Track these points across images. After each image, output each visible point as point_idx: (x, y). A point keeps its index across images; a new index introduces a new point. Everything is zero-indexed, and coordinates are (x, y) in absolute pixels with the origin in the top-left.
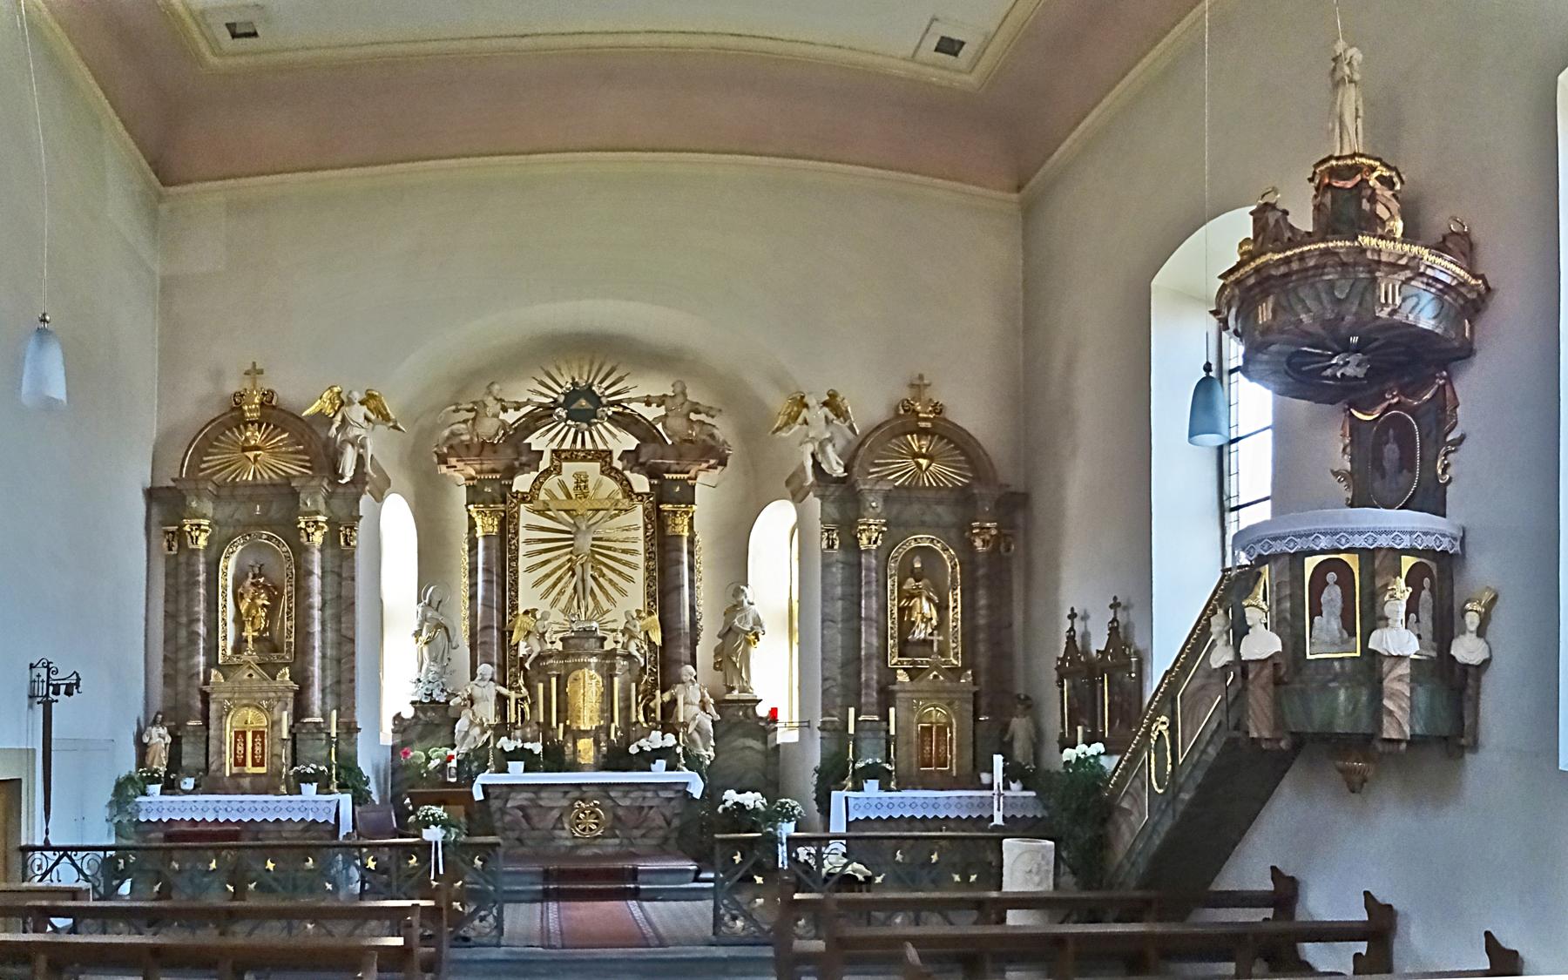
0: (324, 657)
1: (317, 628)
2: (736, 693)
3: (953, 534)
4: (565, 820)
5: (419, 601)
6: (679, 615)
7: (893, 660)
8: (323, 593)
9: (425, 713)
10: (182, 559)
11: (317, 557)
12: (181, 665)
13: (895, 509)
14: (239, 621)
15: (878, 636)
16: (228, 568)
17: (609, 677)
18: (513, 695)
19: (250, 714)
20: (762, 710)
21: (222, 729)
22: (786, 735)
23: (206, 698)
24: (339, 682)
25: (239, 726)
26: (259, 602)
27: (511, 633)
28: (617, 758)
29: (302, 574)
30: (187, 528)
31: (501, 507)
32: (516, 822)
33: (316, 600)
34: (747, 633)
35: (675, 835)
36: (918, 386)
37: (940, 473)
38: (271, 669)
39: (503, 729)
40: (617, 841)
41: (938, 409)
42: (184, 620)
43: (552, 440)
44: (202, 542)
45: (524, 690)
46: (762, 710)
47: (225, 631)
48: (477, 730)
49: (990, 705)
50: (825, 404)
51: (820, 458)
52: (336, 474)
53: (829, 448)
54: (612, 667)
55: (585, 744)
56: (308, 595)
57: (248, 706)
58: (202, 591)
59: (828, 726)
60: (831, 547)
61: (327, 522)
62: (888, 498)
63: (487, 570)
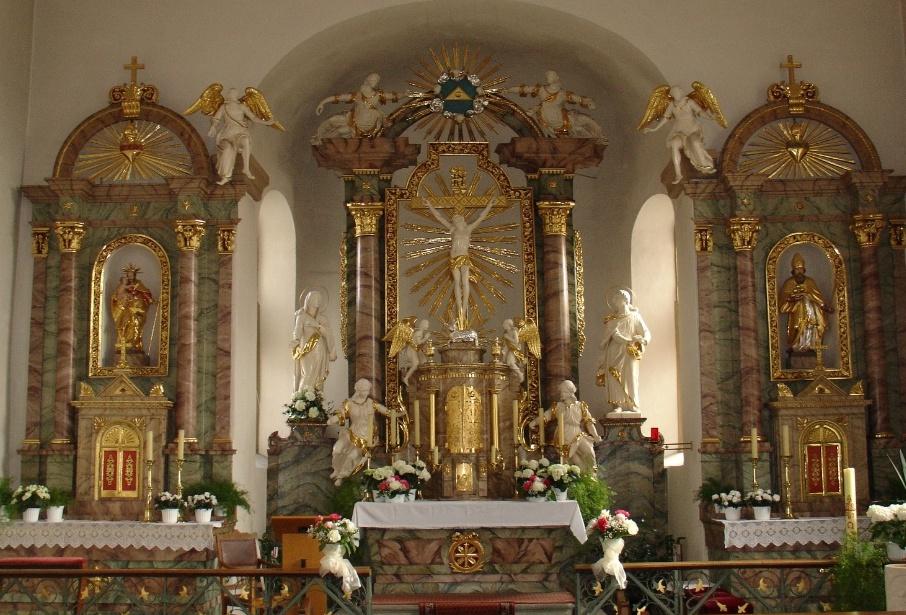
0: (199, 371)
1: (193, 339)
2: (619, 411)
3: (837, 228)
4: (445, 554)
5: (297, 309)
6: (558, 321)
7: (776, 373)
8: (199, 301)
9: (302, 434)
10: (53, 262)
11: (193, 263)
12: (49, 377)
13: (771, 203)
14: (112, 329)
15: (758, 346)
16: (101, 281)
17: (488, 394)
18: (393, 414)
19: (121, 432)
20: (646, 432)
21: (92, 448)
22: (673, 460)
23: (74, 413)
24: (214, 399)
25: (109, 446)
26: (134, 310)
27: (390, 343)
28: (505, 486)
29: (177, 281)
30: (60, 231)
31: (379, 204)
32: (394, 556)
33: (193, 309)
34: (628, 344)
35: (556, 570)
36: (790, 66)
37: (829, 162)
38: (145, 383)
39: (382, 453)
40: (496, 577)
41: (811, 93)
42: (52, 328)
43: (429, 133)
44: (75, 244)
45: (403, 408)
46: (646, 432)
47: (96, 341)
48: (354, 454)
49: (886, 420)
50: (691, 96)
51: (688, 153)
52: (214, 174)
53: (697, 145)
54: (491, 383)
55: (464, 470)
56: (184, 303)
57: (120, 423)
58: (73, 297)
59: (710, 448)
60: (704, 249)
61: (204, 226)
62: (760, 192)
63: (365, 275)
